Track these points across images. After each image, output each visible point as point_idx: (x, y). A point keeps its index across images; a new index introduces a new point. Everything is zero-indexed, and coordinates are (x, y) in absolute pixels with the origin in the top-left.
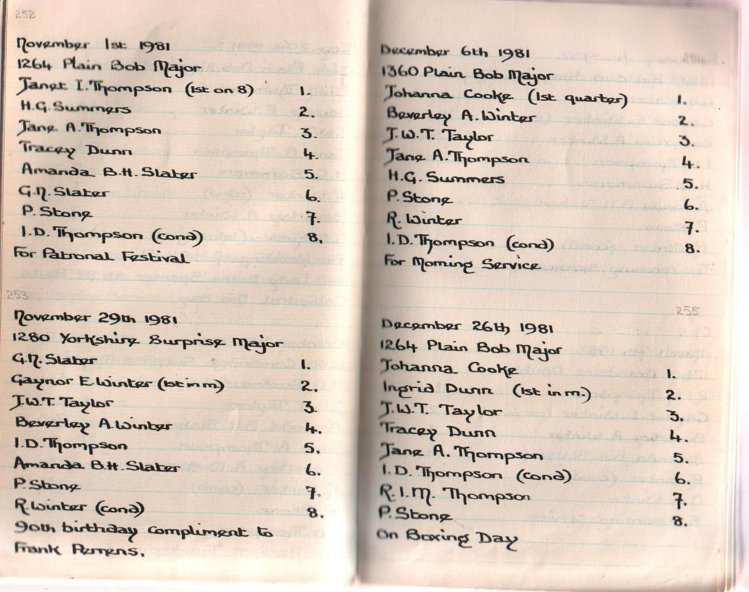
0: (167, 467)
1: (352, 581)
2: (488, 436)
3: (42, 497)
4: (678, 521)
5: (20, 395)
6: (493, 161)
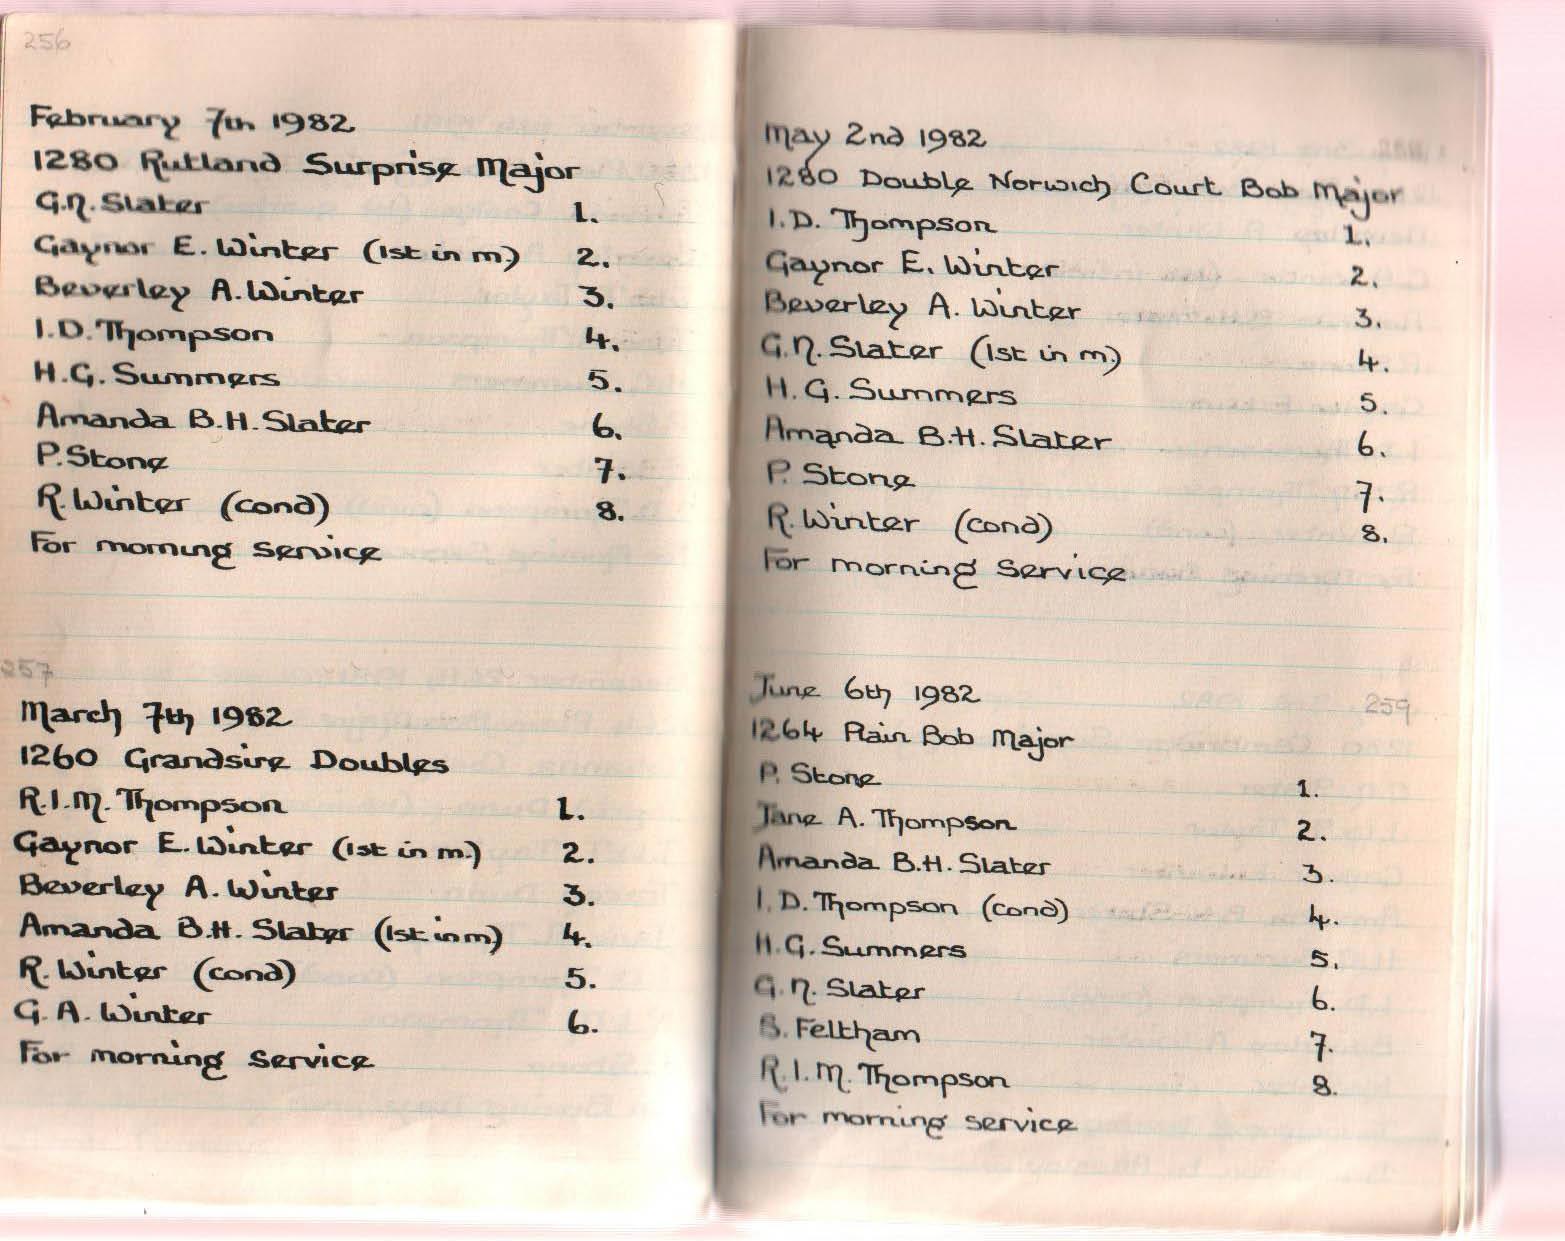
0: (329, 930)
1: (706, 1206)
3: (94, 480)
4: (1321, 1085)
6: (943, 1083)
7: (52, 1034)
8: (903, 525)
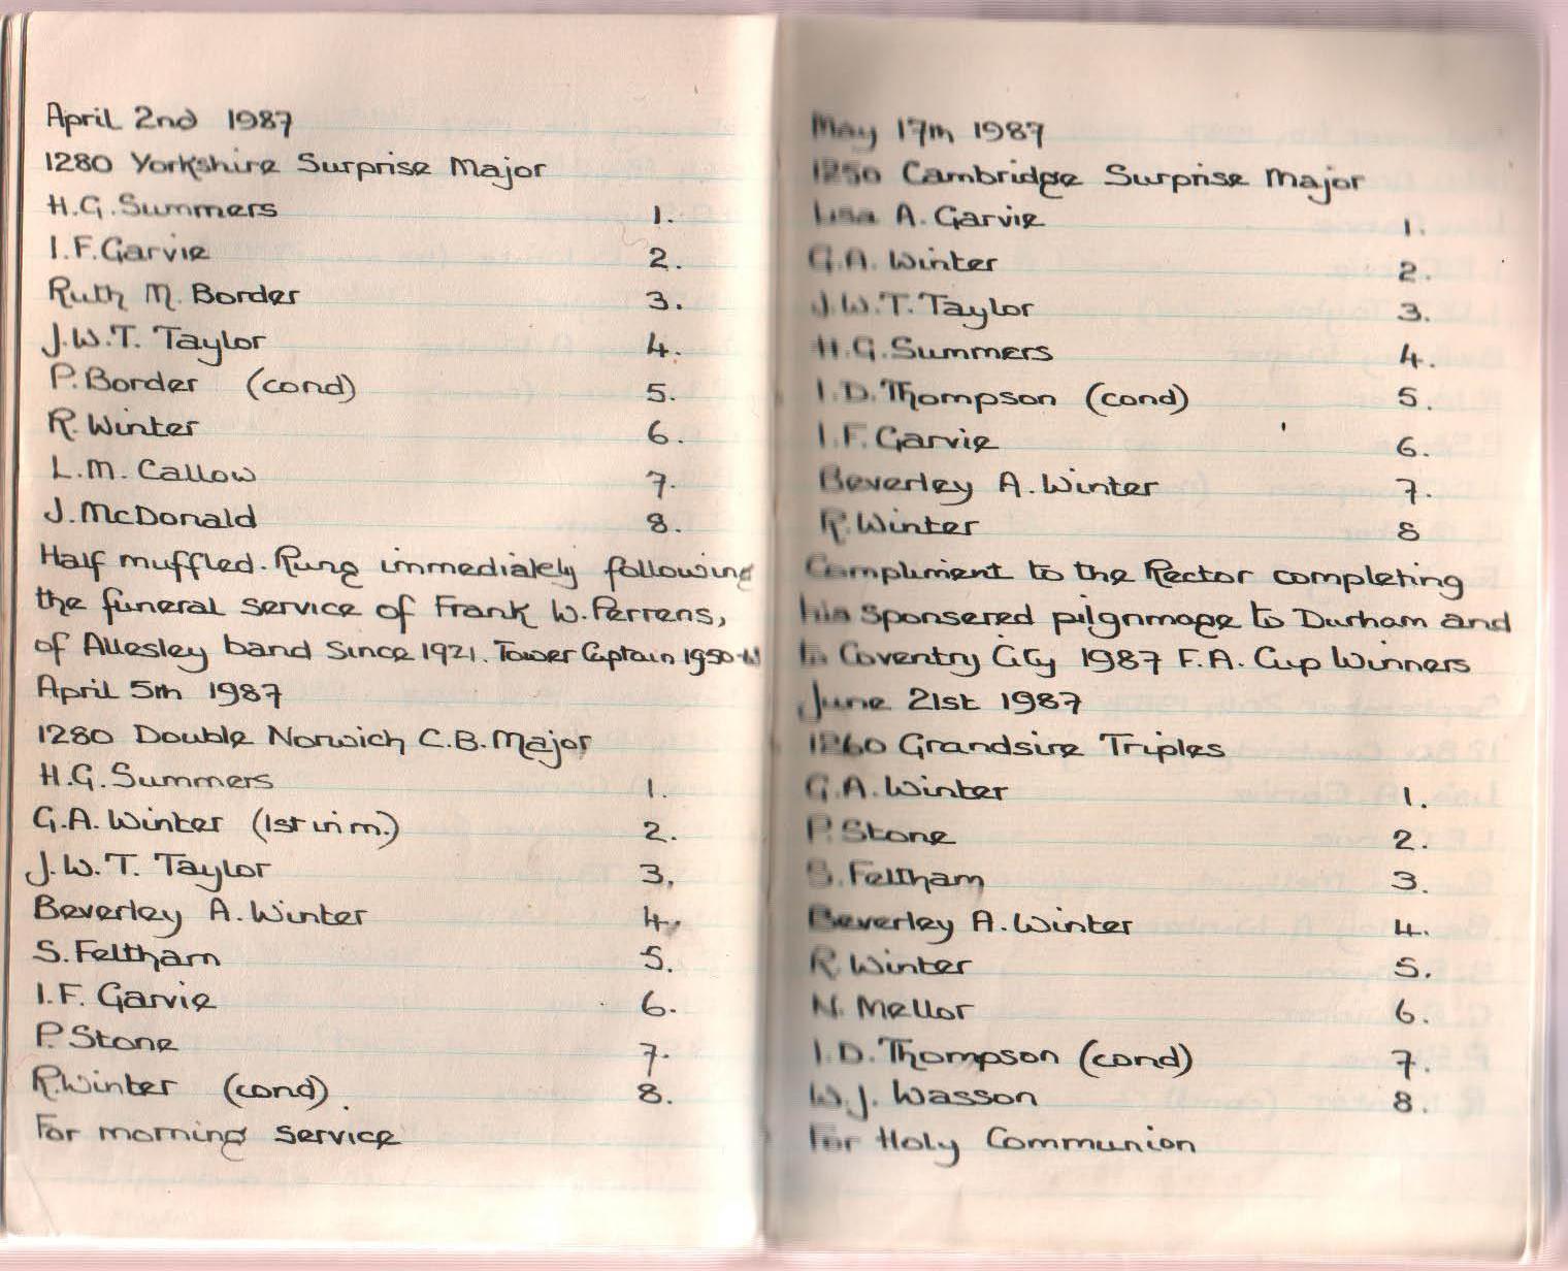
2: (975, 357)
6: (1345, 581)
8: (992, 793)
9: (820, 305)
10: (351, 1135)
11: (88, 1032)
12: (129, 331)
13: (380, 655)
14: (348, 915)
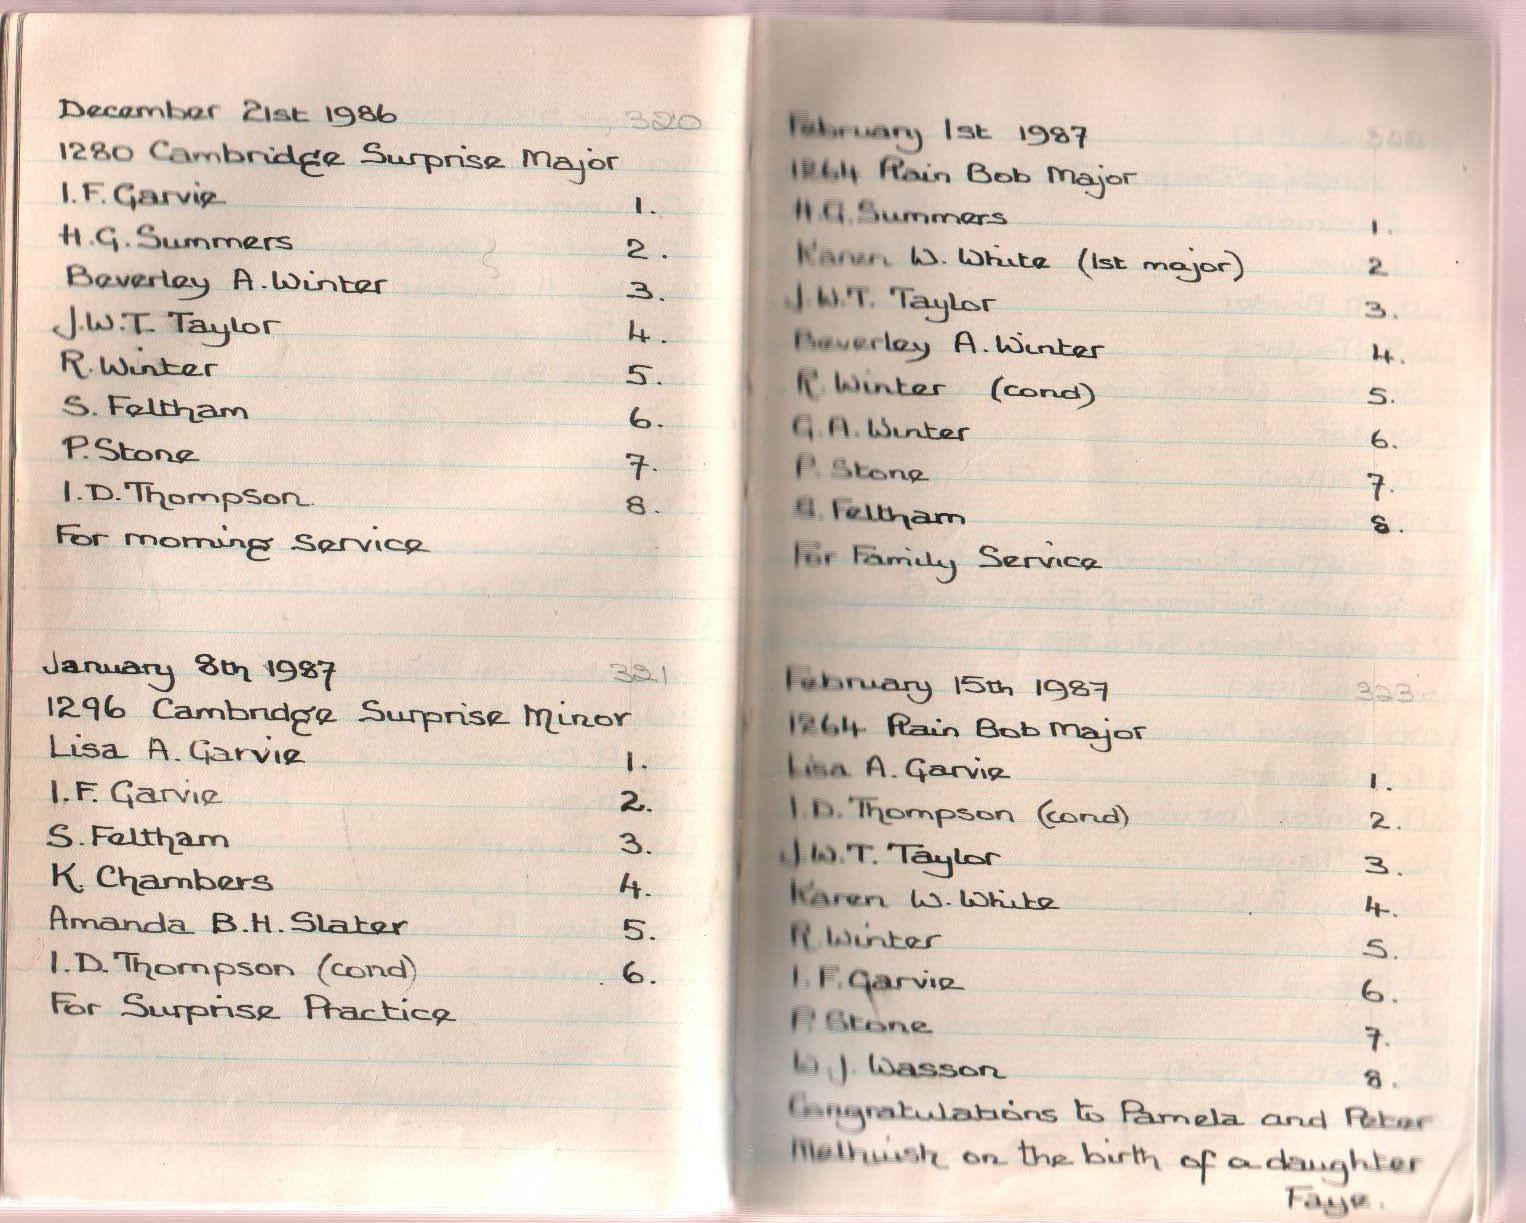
5: (905, 843)
7: (82, 987)
9: (794, 299)
10: (378, 543)
11: (110, 446)
12: (141, 319)
13: (390, 973)
14: (369, 283)
